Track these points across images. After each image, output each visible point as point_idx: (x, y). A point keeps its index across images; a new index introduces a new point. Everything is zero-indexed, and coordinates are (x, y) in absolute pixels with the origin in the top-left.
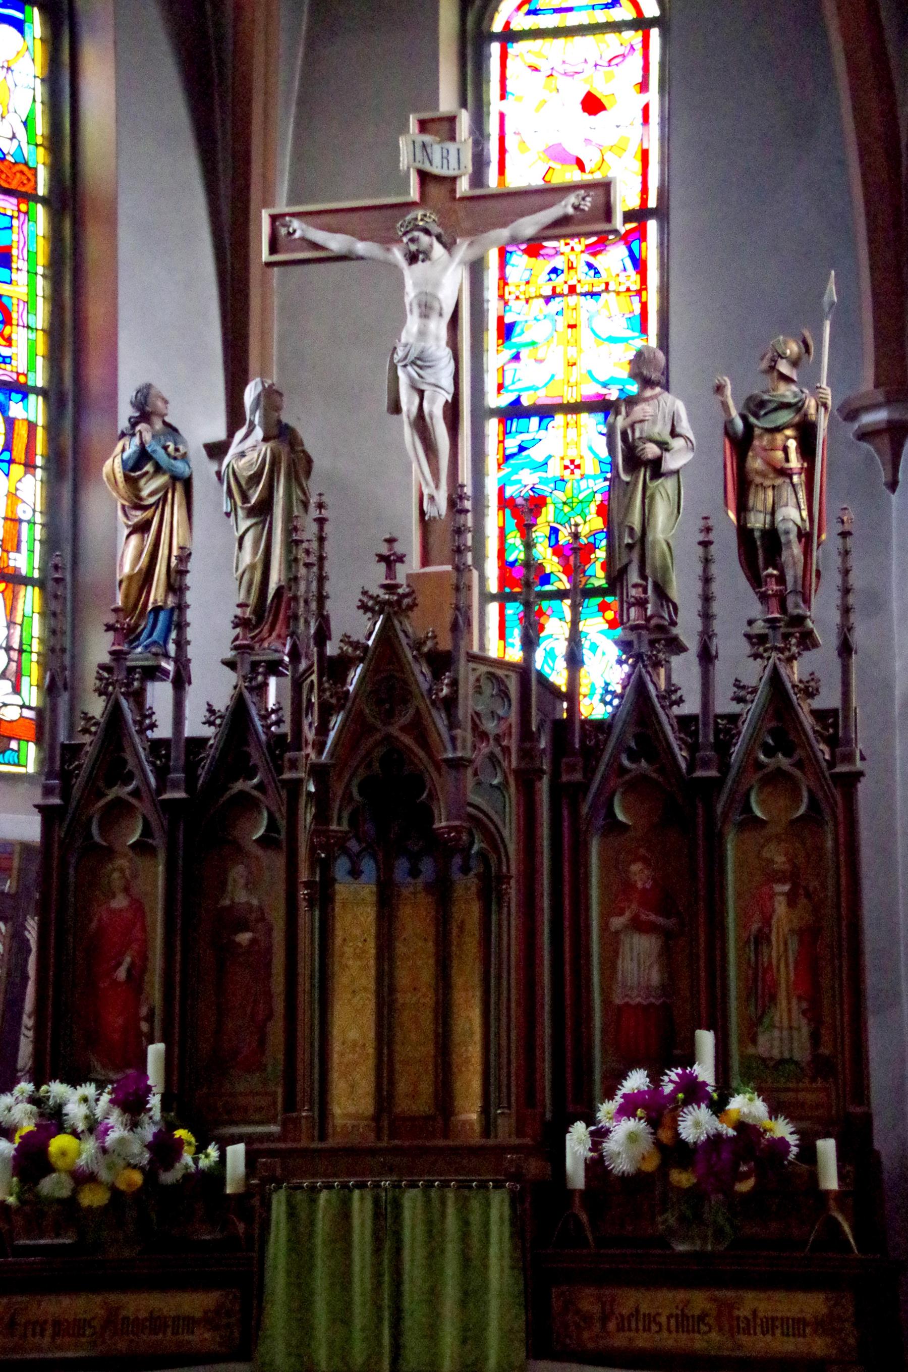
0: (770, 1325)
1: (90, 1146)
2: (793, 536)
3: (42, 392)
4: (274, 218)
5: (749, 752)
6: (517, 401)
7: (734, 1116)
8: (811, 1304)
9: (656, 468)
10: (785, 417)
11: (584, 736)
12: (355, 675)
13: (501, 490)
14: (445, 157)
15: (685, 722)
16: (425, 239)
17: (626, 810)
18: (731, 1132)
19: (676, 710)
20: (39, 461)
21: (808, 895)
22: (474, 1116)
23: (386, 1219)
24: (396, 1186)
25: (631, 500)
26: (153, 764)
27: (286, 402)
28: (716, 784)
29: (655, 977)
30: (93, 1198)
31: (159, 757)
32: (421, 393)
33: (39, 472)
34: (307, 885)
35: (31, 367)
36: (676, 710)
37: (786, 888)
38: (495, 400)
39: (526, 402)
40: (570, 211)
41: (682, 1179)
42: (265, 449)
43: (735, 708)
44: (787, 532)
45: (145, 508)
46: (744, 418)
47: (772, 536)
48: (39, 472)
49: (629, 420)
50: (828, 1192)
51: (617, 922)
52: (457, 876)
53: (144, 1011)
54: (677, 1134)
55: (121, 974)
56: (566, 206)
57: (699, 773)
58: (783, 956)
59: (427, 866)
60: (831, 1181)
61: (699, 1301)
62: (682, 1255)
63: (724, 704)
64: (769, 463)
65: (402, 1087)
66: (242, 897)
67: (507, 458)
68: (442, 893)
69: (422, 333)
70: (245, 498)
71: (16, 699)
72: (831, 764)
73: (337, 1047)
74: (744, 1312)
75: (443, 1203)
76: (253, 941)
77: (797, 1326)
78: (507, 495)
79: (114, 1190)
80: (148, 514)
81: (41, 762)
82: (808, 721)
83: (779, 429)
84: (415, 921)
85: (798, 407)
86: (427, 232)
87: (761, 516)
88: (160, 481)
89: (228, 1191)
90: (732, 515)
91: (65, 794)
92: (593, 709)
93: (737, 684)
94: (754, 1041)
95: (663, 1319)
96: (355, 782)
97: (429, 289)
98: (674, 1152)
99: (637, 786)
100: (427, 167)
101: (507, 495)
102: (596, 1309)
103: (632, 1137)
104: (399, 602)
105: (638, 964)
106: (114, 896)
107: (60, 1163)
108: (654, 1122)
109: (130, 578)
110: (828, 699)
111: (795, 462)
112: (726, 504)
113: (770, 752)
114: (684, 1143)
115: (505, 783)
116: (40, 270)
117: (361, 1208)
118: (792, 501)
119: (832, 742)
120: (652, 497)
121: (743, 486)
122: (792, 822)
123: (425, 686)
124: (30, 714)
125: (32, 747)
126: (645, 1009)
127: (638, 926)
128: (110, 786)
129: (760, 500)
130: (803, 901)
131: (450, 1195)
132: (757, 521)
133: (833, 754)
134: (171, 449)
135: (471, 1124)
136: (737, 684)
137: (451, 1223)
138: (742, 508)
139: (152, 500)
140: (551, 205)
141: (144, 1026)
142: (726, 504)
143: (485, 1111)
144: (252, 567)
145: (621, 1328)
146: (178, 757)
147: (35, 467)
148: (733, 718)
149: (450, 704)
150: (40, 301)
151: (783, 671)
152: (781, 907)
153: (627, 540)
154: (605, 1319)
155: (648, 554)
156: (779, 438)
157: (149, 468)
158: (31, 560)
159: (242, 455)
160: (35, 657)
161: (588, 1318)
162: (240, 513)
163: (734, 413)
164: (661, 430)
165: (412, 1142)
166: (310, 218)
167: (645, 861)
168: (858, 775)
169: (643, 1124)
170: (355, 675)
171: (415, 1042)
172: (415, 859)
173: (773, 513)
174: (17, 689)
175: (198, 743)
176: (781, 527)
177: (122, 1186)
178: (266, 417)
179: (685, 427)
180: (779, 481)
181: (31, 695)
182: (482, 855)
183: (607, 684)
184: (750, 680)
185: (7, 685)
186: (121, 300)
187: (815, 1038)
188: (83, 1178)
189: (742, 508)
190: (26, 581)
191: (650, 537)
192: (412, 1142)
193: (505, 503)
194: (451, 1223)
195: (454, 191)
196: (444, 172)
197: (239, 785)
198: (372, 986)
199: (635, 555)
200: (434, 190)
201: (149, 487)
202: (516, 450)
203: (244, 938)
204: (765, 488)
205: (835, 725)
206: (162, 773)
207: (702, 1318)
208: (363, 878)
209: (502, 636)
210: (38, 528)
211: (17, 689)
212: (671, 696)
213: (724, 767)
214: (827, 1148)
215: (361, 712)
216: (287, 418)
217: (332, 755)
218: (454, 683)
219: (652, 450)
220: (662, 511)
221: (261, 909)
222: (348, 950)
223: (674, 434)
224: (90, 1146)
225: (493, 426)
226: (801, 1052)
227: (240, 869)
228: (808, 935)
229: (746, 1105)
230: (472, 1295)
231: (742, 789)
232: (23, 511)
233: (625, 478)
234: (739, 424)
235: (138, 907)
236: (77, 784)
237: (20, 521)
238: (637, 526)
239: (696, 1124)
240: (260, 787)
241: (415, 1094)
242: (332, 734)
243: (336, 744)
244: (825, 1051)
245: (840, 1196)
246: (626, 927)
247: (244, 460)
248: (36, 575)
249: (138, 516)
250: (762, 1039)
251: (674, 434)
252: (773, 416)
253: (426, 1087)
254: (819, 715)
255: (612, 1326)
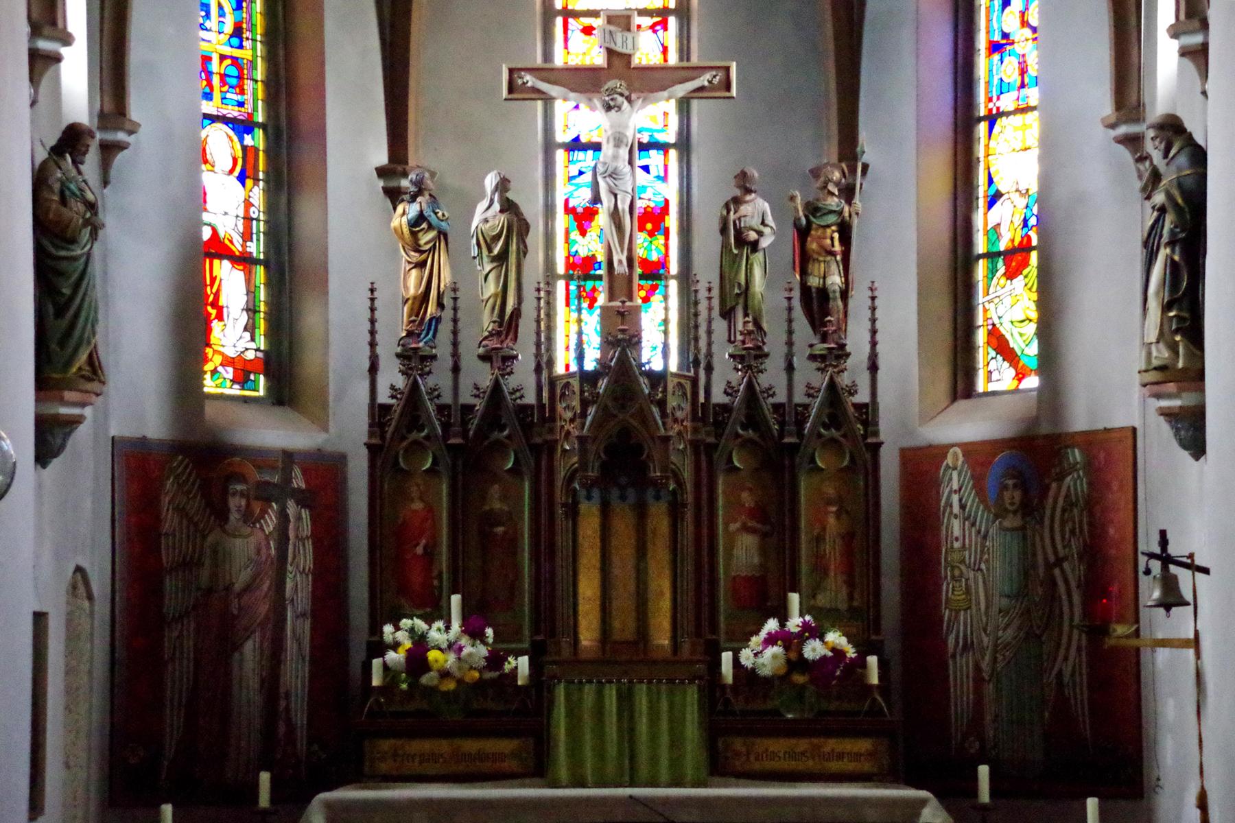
0: (840, 756)
1: (452, 658)
2: (838, 295)
3: (263, 126)
4: (511, 71)
5: (814, 425)
6: (577, 139)
7: (831, 645)
8: (864, 745)
9: (754, 246)
10: (832, 219)
11: (716, 414)
12: (602, 384)
13: (567, 201)
14: (625, 41)
15: (777, 407)
16: (620, 99)
17: (739, 461)
18: (830, 654)
19: (771, 400)
20: (261, 176)
21: (847, 512)
22: (667, 642)
23: (626, 699)
24: (630, 682)
25: (739, 266)
26: (439, 420)
27: (512, 185)
28: (794, 448)
29: (756, 560)
30: (450, 686)
31: (443, 416)
32: (616, 196)
33: (261, 183)
34: (564, 505)
35: (255, 109)
36: (771, 400)
37: (834, 509)
38: (563, 136)
39: (584, 139)
40: (706, 84)
41: (799, 679)
42: (503, 218)
43: (807, 400)
44: (834, 292)
45: (422, 252)
46: (806, 217)
47: (823, 293)
48: (261, 183)
49: (738, 215)
50: (872, 686)
51: (733, 527)
52: (650, 500)
53: (435, 573)
54: (801, 655)
55: (419, 550)
56: (704, 80)
57: (786, 440)
58: (832, 549)
59: (631, 494)
60: (874, 679)
61: (803, 744)
62: (788, 720)
63: (799, 398)
64: (822, 247)
65: (617, 624)
66: (497, 505)
67: (570, 179)
68: (641, 512)
69: (615, 157)
70: (490, 250)
71: (253, 345)
72: (865, 437)
73: (581, 601)
74: (827, 749)
75: (659, 693)
76: (505, 533)
77: (857, 756)
78: (571, 205)
79: (460, 682)
80: (424, 256)
81: (268, 389)
82: (851, 410)
83: (828, 226)
84: (623, 525)
85: (840, 213)
86: (622, 95)
87: (817, 280)
88: (432, 234)
89: (520, 683)
90: (798, 277)
91: (383, 437)
92: (718, 397)
93: (809, 386)
94: (814, 597)
95: (781, 755)
96: (602, 447)
97: (621, 130)
98: (797, 663)
99: (746, 444)
100: (612, 46)
101: (571, 205)
102: (744, 750)
103: (774, 657)
104: (630, 340)
105: (742, 552)
106: (412, 500)
107: (435, 666)
108: (787, 648)
109: (415, 298)
110: (863, 397)
111: (837, 247)
112: (794, 269)
113: (826, 427)
114: (806, 660)
115: (685, 448)
116: (259, 38)
117: (611, 693)
118: (836, 272)
119: (865, 423)
120: (752, 265)
121: (804, 260)
122: (841, 470)
123: (647, 391)
124: (260, 355)
125: (262, 377)
126: (747, 579)
127: (745, 529)
128: (410, 431)
129: (817, 269)
130: (844, 516)
131: (663, 688)
132: (814, 282)
133: (866, 431)
134: (440, 214)
135: (663, 646)
136: (809, 386)
137: (664, 706)
138: (804, 273)
139: (427, 247)
140: (693, 79)
141: (436, 582)
142: (794, 269)
143: (674, 638)
144: (496, 295)
145: (757, 759)
146: (455, 418)
147: (259, 180)
148: (806, 407)
149: (662, 404)
150: (259, 59)
151: (838, 380)
152: (832, 520)
153: (737, 291)
154: (748, 754)
155: (750, 302)
156: (829, 231)
157: (424, 225)
158: (258, 245)
159: (486, 221)
160: (262, 315)
161: (737, 754)
162: (485, 259)
163: (801, 213)
164: (755, 222)
165: (624, 656)
166: (537, 73)
167: (750, 490)
168: (880, 444)
169: (781, 649)
170: (602, 384)
171: (623, 600)
172: (623, 489)
173: (824, 278)
174: (253, 339)
175: (468, 409)
176: (831, 289)
177: (467, 679)
178: (501, 197)
179: (770, 220)
180: (829, 258)
181: (261, 343)
182: (674, 493)
183: (729, 382)
184: (816, 384)
185: (247, 335)
186: (328, 68)
187: (851, 597)
188: (445, 674)
189: (804, 273)
190: (257, 262)
191: (751, 290)
192: (624, 656)
193: (569, 210)
194: (664, 706)
195: (630, 63)
196: (624, 51)
197: (496, 435)
198: (598, 565)
199: (741, 301)
200: (617, 62)
201: (426, 238)
202: (577, 173)
203: (500, 530)
204: (819, 262)
205: (867, 413)
206: (446, 426)
207: (803, 754)
208: (593, 501)
209: (568, 305)
210: (262, 223)
211: (253, 339)
212: (770, 392)
213: (800, 434)
214: (873, 660)
215: (606, 406)
216: (510, 195)
217: (589, 430)
218: (665, 391)
219: (753, 236)
220: (757, 272)
221: (510, 513)
222: (586, 544)
223: (763, 223)
224: (452, 658)
225: (560, 155)
226: (843, 606)
227: (496, 486)
228: (848, 538)
229: (835, 637)
230: (676, 743)
231: (810, 450)
232: (254, 213)
233: (735, 251)
234: (804, 221)
235: (431, 511)
236: (390, 430)
237: (252, 219)
238: (743, 282)
239: (813, 650)
240: (509, 437)
241: (624, 626)
242: (589, 418)
243: (591, 425)
244: (855, 604)
245: (878, 687)
246: (738, 530)
247: (488, 225)
248: (262, 257)
249: (415, 257)
250: (819, 597)
251: (763, 223)
252: (825, 218)
253: (631, 625)
254: (858, 407)
255: (752, 758)
